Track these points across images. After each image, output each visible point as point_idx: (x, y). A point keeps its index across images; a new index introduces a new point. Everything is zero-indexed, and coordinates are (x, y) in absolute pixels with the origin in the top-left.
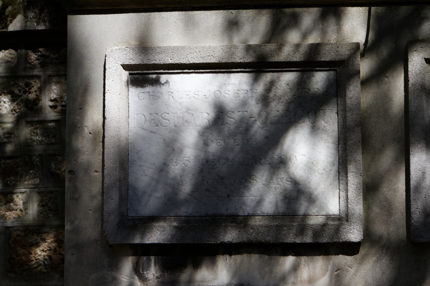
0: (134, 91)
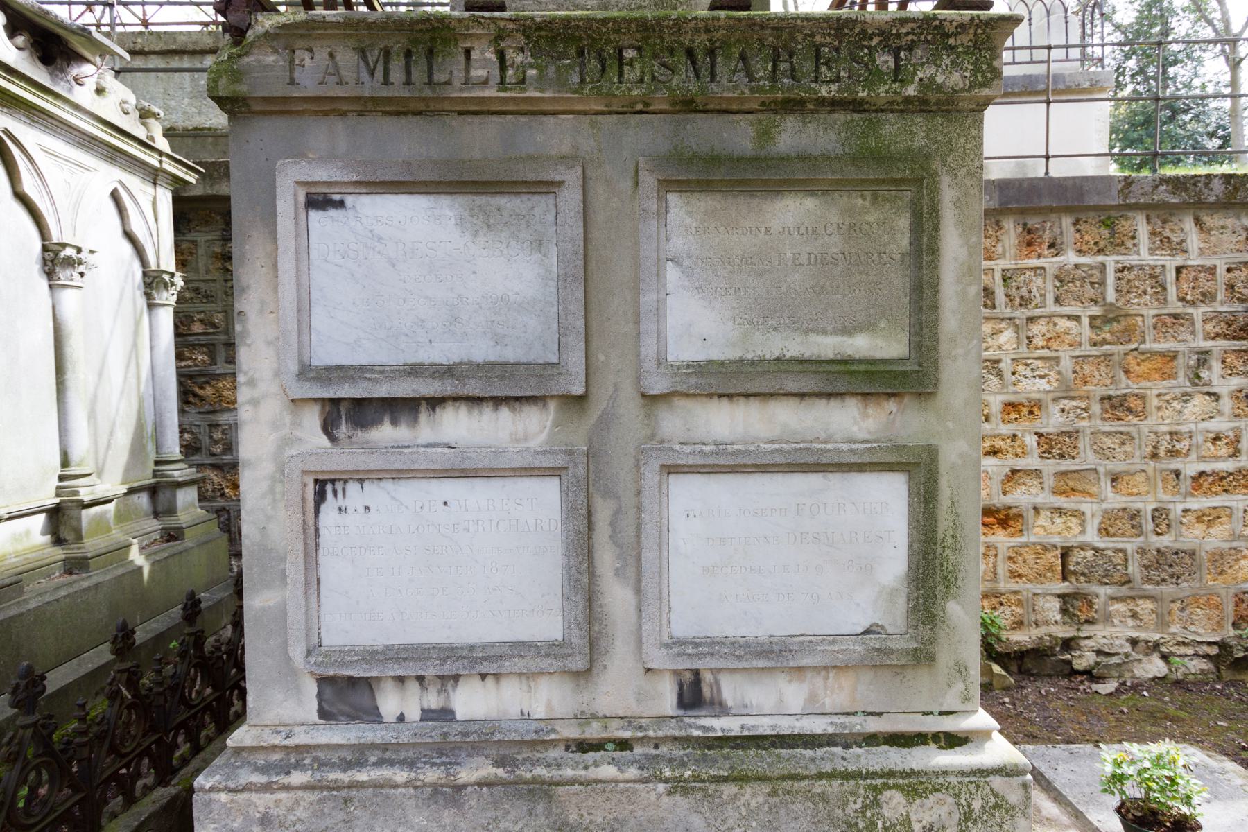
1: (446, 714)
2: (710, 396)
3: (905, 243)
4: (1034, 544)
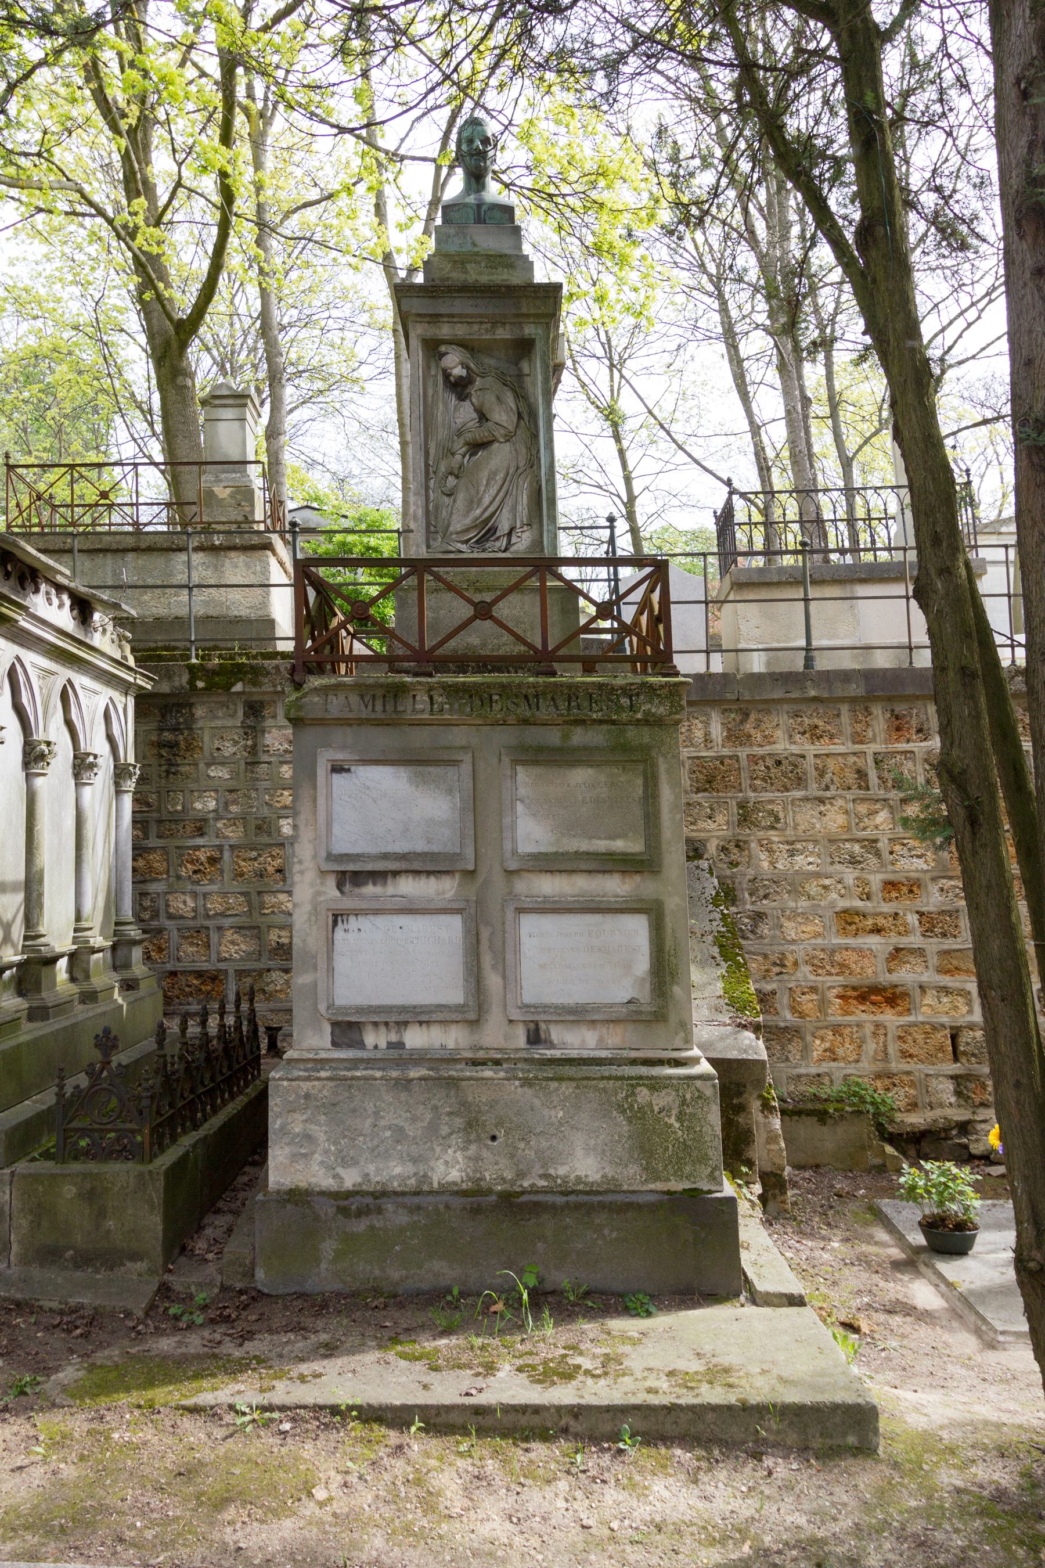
1: (400, 1045)
2: (541, 871)
3: (641, 792)
4: (923, 1023)
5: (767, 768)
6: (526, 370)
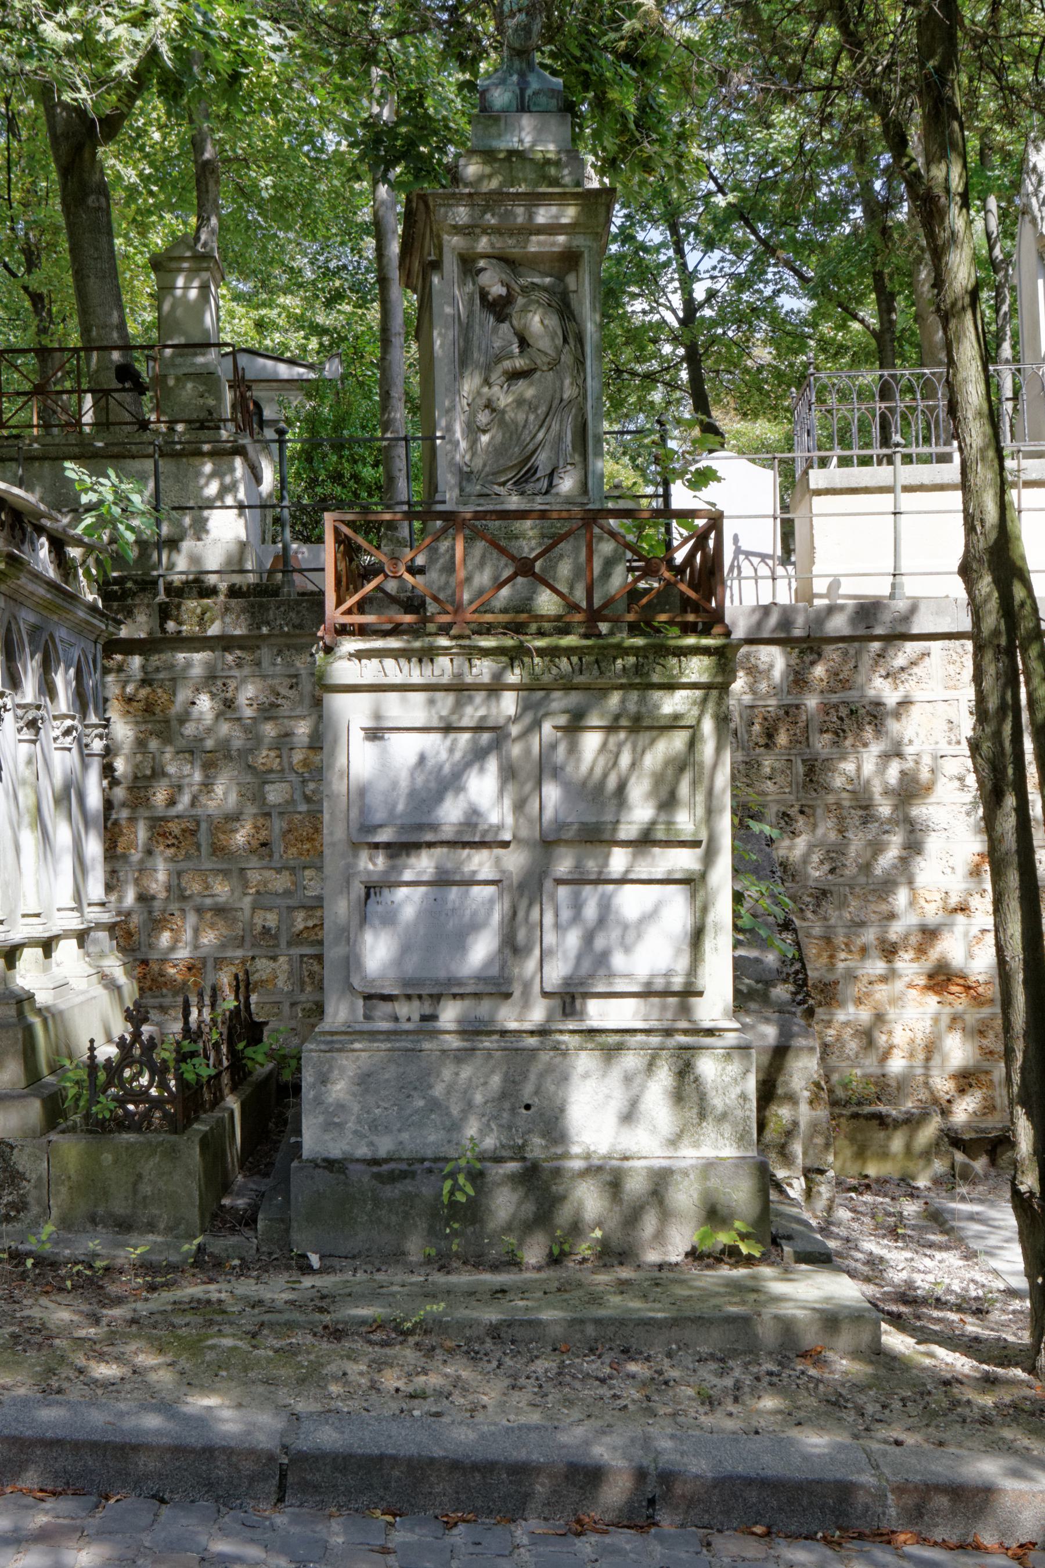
0: (368, 745)
5: (841, 719)
6: (572, 287)
